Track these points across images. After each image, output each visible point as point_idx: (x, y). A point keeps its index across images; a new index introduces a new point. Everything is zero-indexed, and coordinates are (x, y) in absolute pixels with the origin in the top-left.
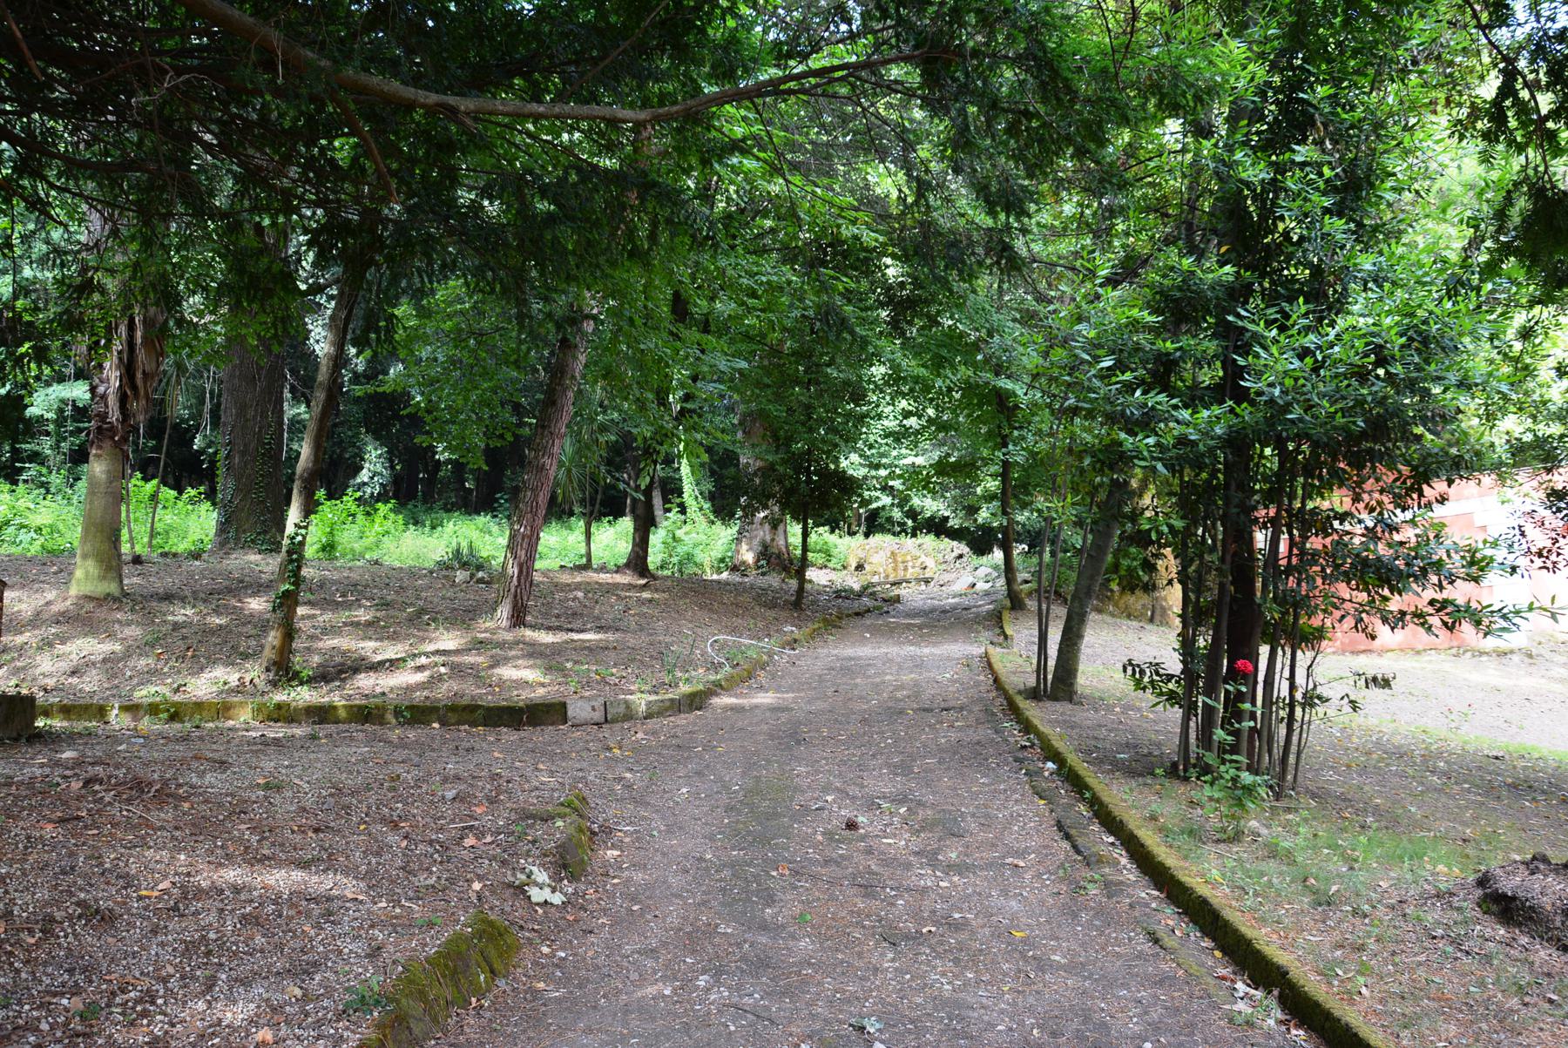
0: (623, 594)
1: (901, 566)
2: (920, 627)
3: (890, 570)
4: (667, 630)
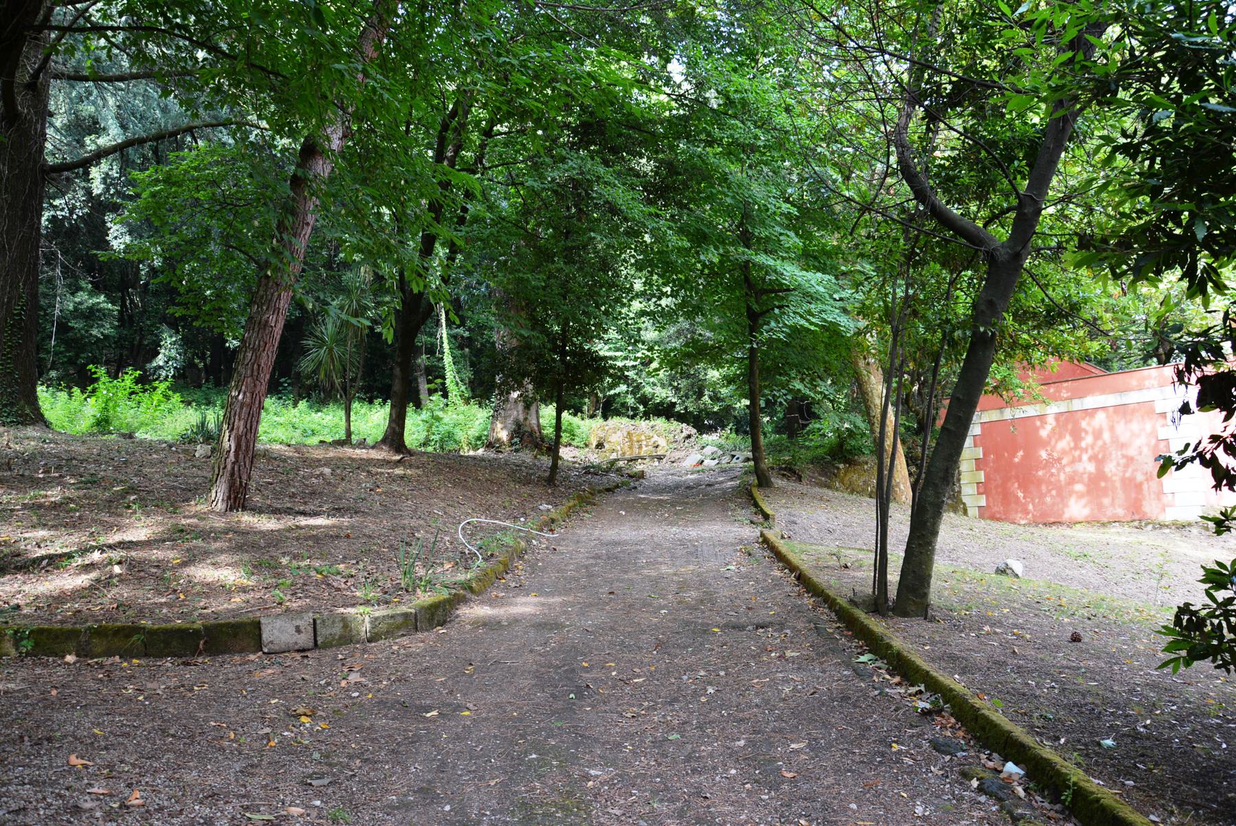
0: (374, 470)
1: (636, 445)
2: (673, 504)
3: (626, 448)
4: (415, 511)
